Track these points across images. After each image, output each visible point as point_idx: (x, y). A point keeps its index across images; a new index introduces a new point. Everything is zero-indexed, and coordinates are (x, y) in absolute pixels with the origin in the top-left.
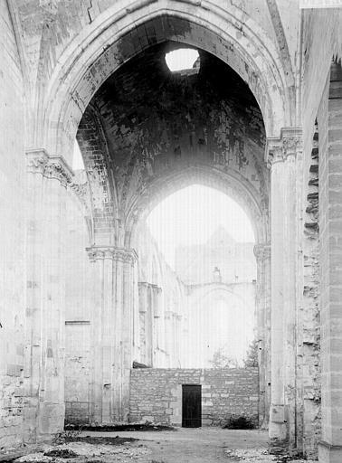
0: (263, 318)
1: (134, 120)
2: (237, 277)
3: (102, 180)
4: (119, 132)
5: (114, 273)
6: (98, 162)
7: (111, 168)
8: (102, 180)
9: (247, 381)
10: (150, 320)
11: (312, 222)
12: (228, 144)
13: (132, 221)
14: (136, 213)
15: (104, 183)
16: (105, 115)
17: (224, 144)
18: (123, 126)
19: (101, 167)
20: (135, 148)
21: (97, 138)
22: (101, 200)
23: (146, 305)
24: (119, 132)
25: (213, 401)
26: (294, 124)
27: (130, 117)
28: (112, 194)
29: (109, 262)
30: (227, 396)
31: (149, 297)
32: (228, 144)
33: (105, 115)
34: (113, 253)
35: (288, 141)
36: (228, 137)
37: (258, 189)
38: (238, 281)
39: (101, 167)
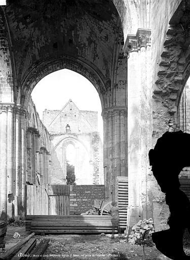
0: (107, 153)
1: (28, 20)
2: (80, 131)
3: (6, 58)
4: (18, 27)
5: (14, 122)
6: (4, 45)
7: (12, 51)
8: (6, 58)
9: (98, 191)
10: (34, 154)
11: (159, 90)
12: (87, 45)
13: (26, 88)
14: (28, 83)
15: (7, 61)
16: (9, 13)
17: (85, 44)
18: (21, 23)
19: (6, 49)
20: (28, 40)
21: (4, 28)
22: (5, 72)
23: (31, 144)
24: (18, 27)
25: (77, 204)
26: (145, 26)
27: (26, 18)
28: (13, 69)
29: (10, 114)
30: (86, 200)
31: (33, 140)
32: (87, 45)
33: (9, 13)
34: (118, 32)
35: (141, 39)
36: (88, 40)
37: (104, 75)
38: (81, 132)
39: (6, 49)
